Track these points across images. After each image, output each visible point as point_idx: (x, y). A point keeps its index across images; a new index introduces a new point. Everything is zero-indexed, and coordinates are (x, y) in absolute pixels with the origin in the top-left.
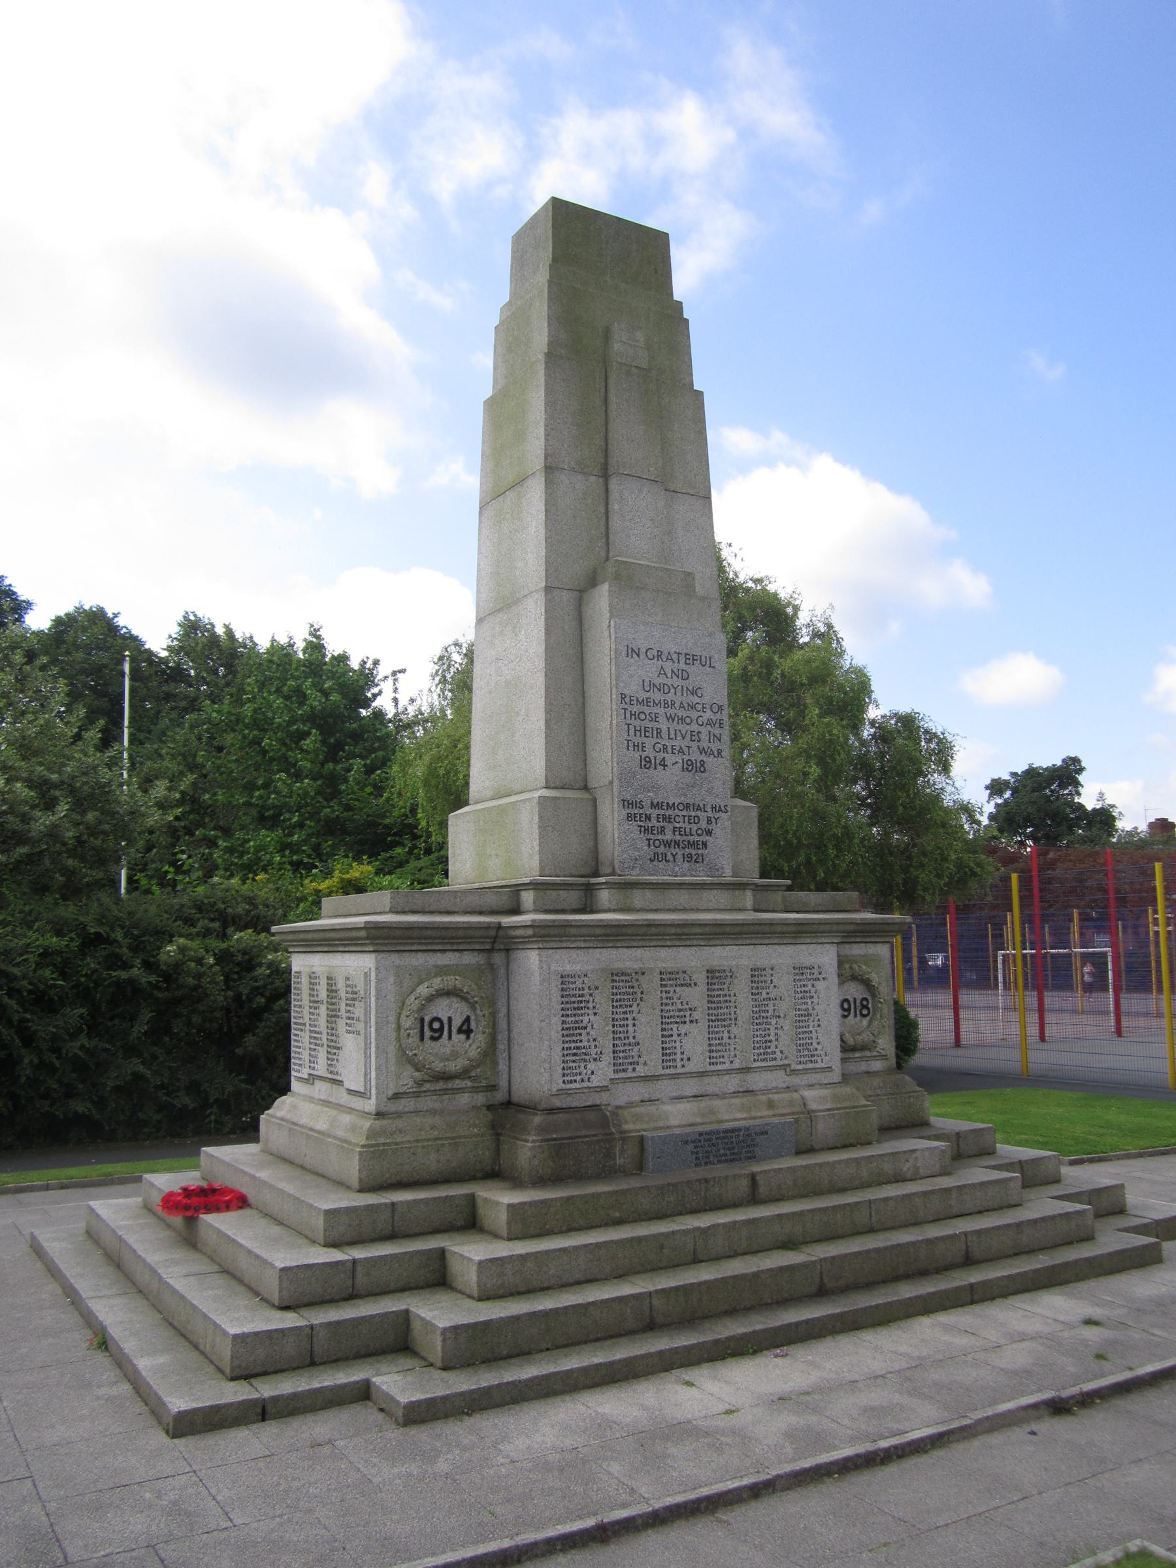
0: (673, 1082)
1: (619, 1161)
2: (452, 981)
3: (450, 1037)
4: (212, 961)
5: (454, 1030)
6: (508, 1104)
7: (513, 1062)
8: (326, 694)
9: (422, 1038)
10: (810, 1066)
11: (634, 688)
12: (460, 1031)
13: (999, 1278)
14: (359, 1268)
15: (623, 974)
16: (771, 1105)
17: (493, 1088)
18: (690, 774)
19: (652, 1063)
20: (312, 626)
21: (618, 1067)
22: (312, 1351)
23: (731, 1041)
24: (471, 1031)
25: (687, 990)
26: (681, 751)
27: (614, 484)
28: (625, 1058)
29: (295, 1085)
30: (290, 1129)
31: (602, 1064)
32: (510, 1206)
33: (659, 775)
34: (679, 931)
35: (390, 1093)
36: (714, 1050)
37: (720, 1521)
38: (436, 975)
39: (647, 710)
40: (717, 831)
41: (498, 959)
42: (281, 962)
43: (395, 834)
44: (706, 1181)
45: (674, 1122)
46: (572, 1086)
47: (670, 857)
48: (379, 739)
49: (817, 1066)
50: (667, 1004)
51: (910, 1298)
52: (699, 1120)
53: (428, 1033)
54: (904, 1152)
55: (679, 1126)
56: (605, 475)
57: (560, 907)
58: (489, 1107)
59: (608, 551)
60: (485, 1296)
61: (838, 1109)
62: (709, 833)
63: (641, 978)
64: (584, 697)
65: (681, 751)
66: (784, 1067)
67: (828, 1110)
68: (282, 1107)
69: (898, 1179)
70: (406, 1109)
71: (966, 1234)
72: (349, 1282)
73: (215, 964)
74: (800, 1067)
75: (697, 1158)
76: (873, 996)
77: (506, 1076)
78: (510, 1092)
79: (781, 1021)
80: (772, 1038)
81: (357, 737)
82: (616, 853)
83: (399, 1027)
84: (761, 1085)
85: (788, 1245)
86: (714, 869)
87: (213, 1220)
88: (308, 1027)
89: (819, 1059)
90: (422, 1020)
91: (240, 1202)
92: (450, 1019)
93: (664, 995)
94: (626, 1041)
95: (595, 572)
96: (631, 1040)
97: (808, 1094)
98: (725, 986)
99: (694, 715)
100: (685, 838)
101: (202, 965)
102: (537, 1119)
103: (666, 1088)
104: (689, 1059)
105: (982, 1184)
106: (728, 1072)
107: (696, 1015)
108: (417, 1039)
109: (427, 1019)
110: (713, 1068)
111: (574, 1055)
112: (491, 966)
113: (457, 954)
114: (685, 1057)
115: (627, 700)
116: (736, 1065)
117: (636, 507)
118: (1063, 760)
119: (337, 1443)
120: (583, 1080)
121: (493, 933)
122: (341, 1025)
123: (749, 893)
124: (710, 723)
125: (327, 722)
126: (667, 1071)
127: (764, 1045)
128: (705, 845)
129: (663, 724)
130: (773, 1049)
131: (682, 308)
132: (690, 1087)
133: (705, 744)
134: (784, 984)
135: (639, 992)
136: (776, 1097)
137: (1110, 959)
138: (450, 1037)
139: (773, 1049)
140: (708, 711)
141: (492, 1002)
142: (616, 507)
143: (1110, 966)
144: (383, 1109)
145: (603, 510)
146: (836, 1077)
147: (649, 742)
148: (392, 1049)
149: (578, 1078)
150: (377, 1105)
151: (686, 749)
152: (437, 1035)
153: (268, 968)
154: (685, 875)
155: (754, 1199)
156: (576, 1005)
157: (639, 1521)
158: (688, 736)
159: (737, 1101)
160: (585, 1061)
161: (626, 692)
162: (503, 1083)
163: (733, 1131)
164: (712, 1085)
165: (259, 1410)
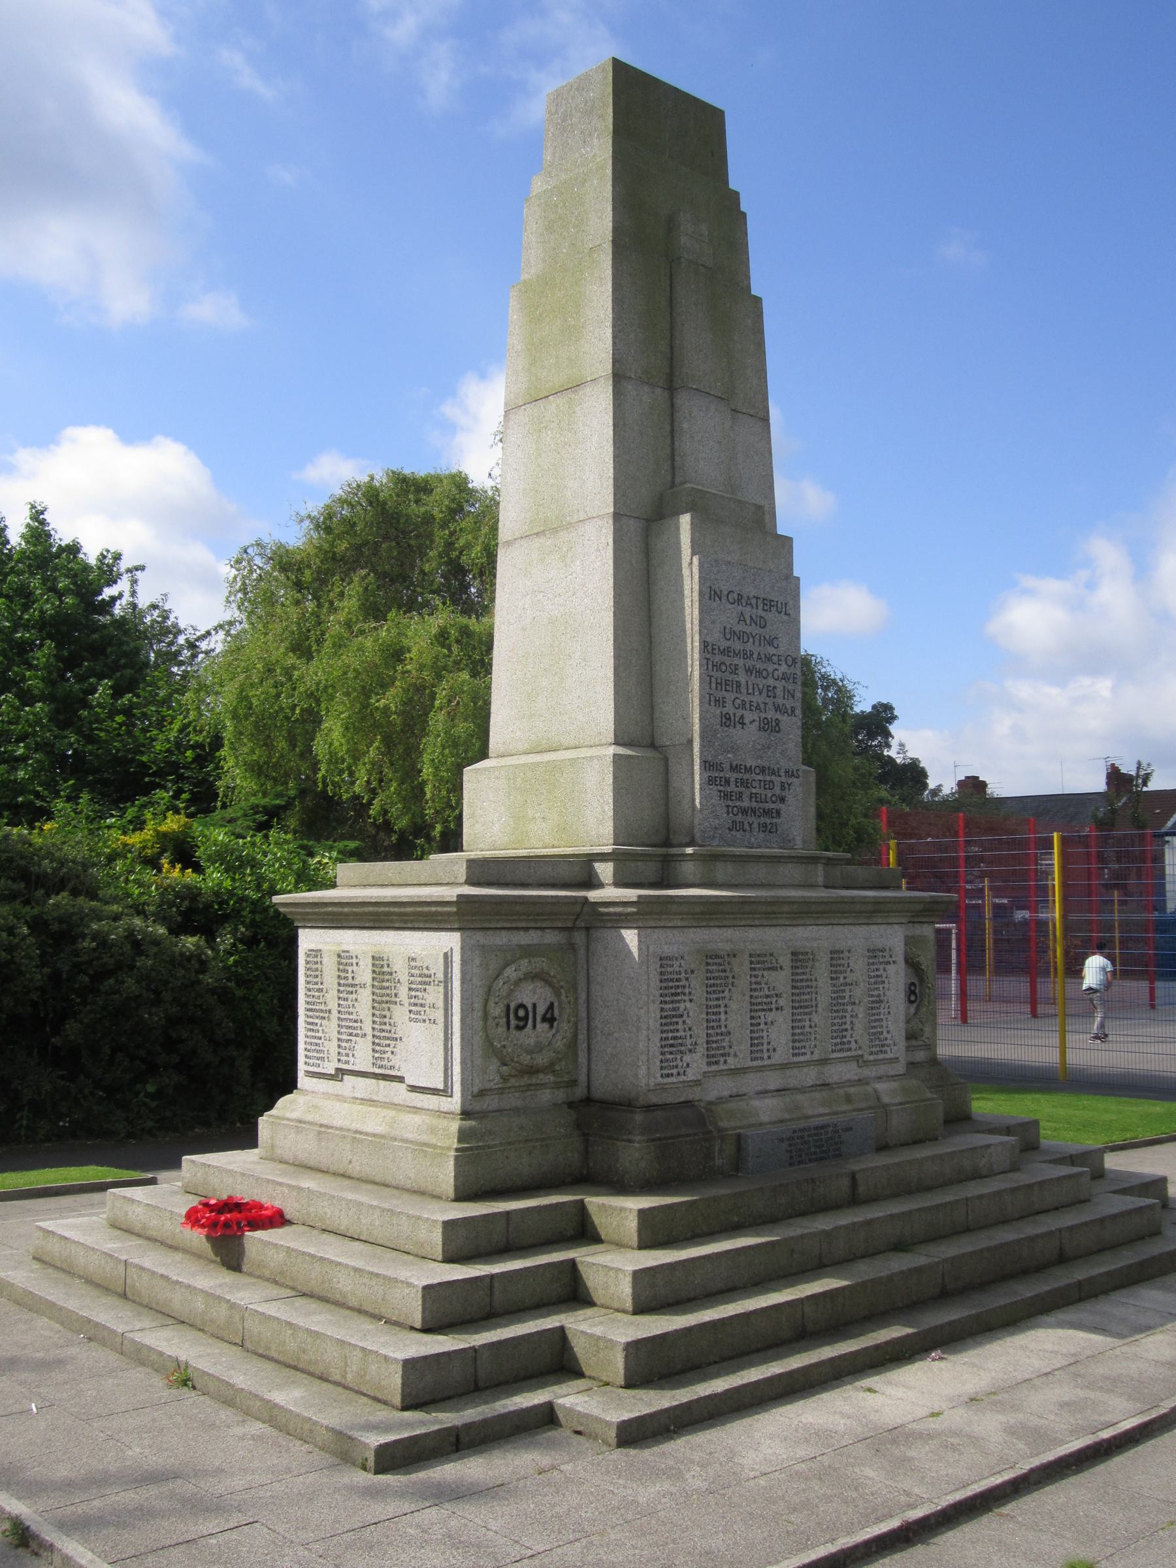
0: (758, 1075)
1: (718, 1162)
2: (540, 963)
3: (534, 1026)
4: (25, 930)
5: (539, 1019)
6: (588, 1100)
7: (594, 1055)
8: (60, 595)
9: (508, 1028)
10: (881, 1056)
11: (716, 635)
12: (544, 1019)
13: (1100, 1274)
14: (496, 1285)
15: (717, 956)
16: (848, 1099)
17: (573, 1083)
18: (766, 734)
19: (740, 1055)
20: (33, 507)
21: (712, 1060)
22: (476, 1376)
23: (812, 1030)
24: (555, 1019)
25: (774, 973)
26: (758, 708)
27: (682, 399)
28: (718, 1048)
29: (303, 1080)
30: (319, 1133)
31: (697, 1056)
32: (642, 1213)
33: (737, 733)
34: (769, 909)
35: (476, 1090)
36: (798, 1040)
37: (1001, 1515)
38: (521, 957)
39: (728, 661)
40: (790, 799)
41: (579, 938)
42: (109, 933)
43: (155, 774)
44: (813, 1181)
45: (765, 1118)
46: (670, 1080)
47: (747, 827)
48: (126, 654)
49: (887, 1056)
50: (755, 990)
51: (1031, 1298)
52: (786, 1116)
53: (513, 1022)
54: (981, 1147)
55: (770, 1123)
56: (671, 389)
57: (638, 881)
58: (570, 1105)
59: (673, 477)
60: (641, 1308)
61: (908, 1103)
62: (782, 800)
63: (733, 960)
64: (651, 642)
65: (758, 708)
66: (857, 1059)
67: (901, 1104)
68: (286, 1106)
69: (977, 1175)
70: (491, 1108)
71: (1060, 1230)
72: (488, 1299)
73: (29, 935)
74: (872, 1058)
75: (791, 1157)
76: (922, 980)
77: (585, 1070)
78: (589, 1087)
79: (856, 1008)
80: (848, 1026)
81: (97, 650)
82: (696, 822)
83: (486, 1016)
84: (835, 1078)
85: (900, 1246)
86: (786, 842)
87: (255, 1240)
88: (335, 1014)
89: (888, 1049)
90: (508, 1007)
91: (277, 1219)
92: (534, 1006)
93: (753, 980)
94: (718, 1031)
95: (661, 497)
96: (723, 1029)
97: (881, 1086)
98: (808, 970)
99: (771, 668)
100: (760, 805)
101: (14, 935)
102: (639, 1118)
103: (751, 1083)
104: (774, 1050)
105: (1058, 1179)
106: (808, 1063)
107: (782, 1002)
108: (505, 1028)
109: (513, 1006)
110: (796, 1059)
111: (672, 1046)
112: (572, 947)
113: (539, 933)
114: (770, 1047)
115: (710, 648)
116: (816, 1057)
117: (702, 424)
118: (874, 707)
119: (562, 1467)
120: (679, 1074)
121: (578, 909)
122: (400, 1014)
123: (820, 867)
124: (785, 677)
125: (57, 628)
126: (755, 1063)
127: (840, 1033)
128: (778, 813)
129: (742, 678)
130: (848, 1038)
131: (738, 200)
132: (773, 1081)
133: (780, 701)
134: (858, 966)
135: (730, 975)
136: (852, 1090)
137: (954, 936)
138: (534, 1026)
139: (848, 1038)
140: (783, 663)
141: (574, 987)
142: (685, 426)
143: (954, 945)
144: (469, 1108)
145: (668, 428)
146: (900, 1068)
147: (730, 697)
148: (478, 1040)
149: (675, 1071)
150: (463, 1103)
151: (762, 706)
152: (521, 1024)
153: (93, 939)
154: (760, 847)
155: (854, 1200)
156: (673, 991)
157: (933, 1521)
158: (765, 691)
159: (817, 1095)
160: (681, 1052)
161: (709, 639)
162: (583, 1078)
163: (822, 1127)
164: (796, 1078)
165: (453, 1439)
